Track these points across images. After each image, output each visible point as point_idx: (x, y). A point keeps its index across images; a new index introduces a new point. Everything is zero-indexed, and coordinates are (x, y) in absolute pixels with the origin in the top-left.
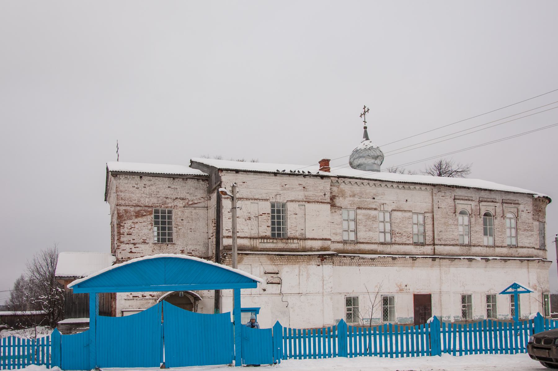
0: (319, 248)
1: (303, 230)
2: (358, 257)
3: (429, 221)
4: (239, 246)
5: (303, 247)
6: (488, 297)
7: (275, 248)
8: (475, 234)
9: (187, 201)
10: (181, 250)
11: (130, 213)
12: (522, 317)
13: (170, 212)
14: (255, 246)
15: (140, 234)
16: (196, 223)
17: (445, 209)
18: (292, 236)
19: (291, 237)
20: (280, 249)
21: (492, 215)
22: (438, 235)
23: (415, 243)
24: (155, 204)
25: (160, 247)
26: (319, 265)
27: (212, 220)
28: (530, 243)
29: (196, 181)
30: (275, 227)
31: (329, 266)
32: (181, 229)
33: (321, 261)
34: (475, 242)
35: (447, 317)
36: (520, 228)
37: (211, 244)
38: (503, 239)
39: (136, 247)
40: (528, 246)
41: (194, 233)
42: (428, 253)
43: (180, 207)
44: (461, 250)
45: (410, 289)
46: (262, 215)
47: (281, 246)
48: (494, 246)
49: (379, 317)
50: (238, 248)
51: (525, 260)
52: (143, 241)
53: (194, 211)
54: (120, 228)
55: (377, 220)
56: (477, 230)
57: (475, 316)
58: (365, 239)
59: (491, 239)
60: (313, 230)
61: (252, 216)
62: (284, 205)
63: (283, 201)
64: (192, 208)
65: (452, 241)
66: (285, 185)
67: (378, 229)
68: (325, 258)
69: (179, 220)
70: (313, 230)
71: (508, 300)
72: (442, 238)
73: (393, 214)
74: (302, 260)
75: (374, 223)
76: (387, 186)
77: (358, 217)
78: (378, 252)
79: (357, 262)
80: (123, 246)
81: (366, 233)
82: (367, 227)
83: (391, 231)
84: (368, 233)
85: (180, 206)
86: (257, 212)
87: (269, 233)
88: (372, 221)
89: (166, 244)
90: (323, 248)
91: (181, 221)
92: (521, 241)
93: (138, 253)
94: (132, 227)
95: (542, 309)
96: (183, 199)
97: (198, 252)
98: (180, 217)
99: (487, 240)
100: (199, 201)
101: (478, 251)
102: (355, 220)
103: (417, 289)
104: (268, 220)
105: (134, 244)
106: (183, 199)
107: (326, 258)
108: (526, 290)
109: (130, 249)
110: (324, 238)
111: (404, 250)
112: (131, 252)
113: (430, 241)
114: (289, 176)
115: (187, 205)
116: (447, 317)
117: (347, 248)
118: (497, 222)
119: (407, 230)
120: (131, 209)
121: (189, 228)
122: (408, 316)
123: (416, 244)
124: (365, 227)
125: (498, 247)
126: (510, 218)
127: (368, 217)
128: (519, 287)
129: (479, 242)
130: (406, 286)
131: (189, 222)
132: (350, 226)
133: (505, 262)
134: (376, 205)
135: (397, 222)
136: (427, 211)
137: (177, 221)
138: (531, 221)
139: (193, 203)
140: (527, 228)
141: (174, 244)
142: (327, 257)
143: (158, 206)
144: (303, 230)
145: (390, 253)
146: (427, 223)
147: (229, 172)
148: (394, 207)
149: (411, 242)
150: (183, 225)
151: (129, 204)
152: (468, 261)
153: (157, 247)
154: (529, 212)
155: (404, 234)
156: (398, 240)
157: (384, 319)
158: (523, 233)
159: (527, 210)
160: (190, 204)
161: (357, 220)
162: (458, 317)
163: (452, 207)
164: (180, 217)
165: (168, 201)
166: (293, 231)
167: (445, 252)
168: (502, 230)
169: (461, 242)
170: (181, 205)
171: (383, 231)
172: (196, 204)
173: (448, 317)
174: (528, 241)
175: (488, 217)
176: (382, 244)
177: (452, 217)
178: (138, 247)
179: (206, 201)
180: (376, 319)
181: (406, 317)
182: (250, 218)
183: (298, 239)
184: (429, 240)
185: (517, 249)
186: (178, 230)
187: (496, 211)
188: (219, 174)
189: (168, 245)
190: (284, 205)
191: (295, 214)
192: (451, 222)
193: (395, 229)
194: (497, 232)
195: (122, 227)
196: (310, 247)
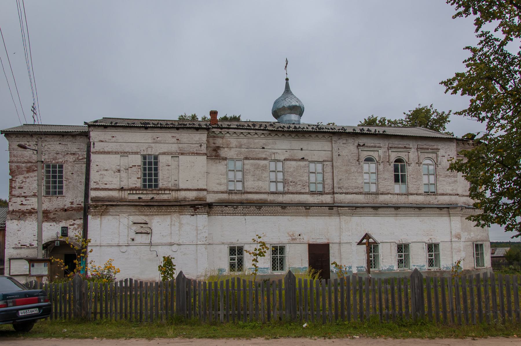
0: (194, 198)
1: (176, 181)
2: (241, 207)
3: (328, 169)
5: (175, 198)
6: (477, 246)
9: (77, 156)
10: (70, 202)
11: (22, 168)
12: (442, 267)
13: (61, 167)
14: (123, 197)
15: (31, 188)
17: (347, 157)
18: (164, 187)
19: (163, 188)
21: (405, 161)
22: (338, 183)
23: (311, 191)
24: (46, 160)
25: (50, 199)
26: (193, 215)
28: (453, 190)
31: (204, 216)
36: (440, 174)
38: (418, 186)
39: (27, 200)
40: (451, 192)
42: (327, 201)
43: (71, 162)
44: (366, 198)
45: (304, 239)
46: (132, 168)
48: (408, 194)
49: (267, 267)
52: (33, 194)
54: (12, 182)
55: (267, 170)
56: (386, 177)
57: (383, 267)
59: (403, 186)
60: (187, 181)
61: (122, 169)
62: (156, 158)
63: (155, 153)
65: (355, 189)
66: (157, 138)
68: (197, 208)
69: (69, 174)
70: (187, 181)
71: (425, 249)
72: (343, 186)
73: (285, 163)
75: (264, 172)
76: (278, 135)
79: (242, 211)
80: (14, 199)
82: (255, 176)
84: (257, 183)
85: (70, 161)
86: (127, 165)
87: (139, 184)
88: (261, 170)
89: (56, 196)
90: (198, 199)
91: (71, 175)
92: (442, 188)
93: (28, 205)
94: (24, 181)
95: (473, 260)
96: (74, 154)
98: (70, 171)
99: (398, 188)
101: (387, 199)
102: (242, 171)
103: (313, 239)
104: (139, 172)
105: (25, 197)
106: (74, 154)
107: (198, 208)
109: (21, 201)
111: (299, 199)
112: (22, 204)
113: (329, 189)
120: (23, 165)
121: (79, 181)
122: (302, 266)
123: (312, 193)
124: (253, 176)
125: (412, 194)
126: (428, 165)
127: (257, 167)
129: (389, 190)
130: (300, 235)
135: (290, 171)
136: (326, 159)
141: (64, 196)
143: (49, 162)
144: (176, 181)
145: (282, 202)
146: (327, 172)
148: (287, 155)
149: (307, 191)
150: (73, 179)
151: (21, 160)
153: (47, 199)
156: (291, 189)
157: (273, 268)
158: (443, 179)
162: (362, 267)
163: (355, 155)
164: (70, 171)
165: (58, 156)
167: (347, 201)
169: (366, 190)
170: (71, 160)
173: (348, 267)
174: (450, 188)
175: (399, 164)
177: (355, 164)
178: (28, 200)
180: (264, 268)
181: (299, 267)
182: (119, 170)
183: (170, 190)
184: (328, 189)
185: (436, 196)
186: (68, 183)
187: (410, 157)
189: (58, 198)
191: (167, 165)
192: (353, 169)
194: (411, 179)
195: (13, 182)
196: (183, 197)
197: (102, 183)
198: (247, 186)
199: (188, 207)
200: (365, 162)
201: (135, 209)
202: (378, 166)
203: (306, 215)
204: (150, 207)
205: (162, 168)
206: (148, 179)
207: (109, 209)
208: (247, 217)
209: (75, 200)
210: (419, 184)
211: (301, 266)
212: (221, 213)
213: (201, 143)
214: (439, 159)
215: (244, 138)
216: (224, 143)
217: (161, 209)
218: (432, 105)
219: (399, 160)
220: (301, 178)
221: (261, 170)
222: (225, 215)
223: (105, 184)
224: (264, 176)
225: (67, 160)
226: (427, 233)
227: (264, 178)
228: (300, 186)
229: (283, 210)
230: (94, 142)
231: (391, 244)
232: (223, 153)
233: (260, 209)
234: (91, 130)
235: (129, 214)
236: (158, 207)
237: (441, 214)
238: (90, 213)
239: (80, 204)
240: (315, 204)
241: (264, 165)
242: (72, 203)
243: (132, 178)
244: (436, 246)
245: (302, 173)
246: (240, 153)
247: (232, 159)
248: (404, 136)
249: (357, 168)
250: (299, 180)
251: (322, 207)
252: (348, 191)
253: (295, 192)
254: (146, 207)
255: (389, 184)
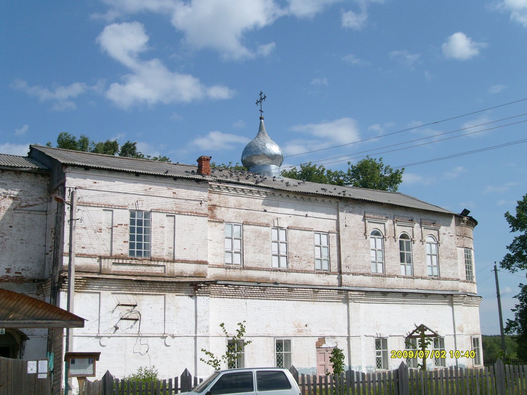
0: (192, 273)
1: (171, 248)
2: (243, 287)
4: (85, 267)
5: (170, 271)
7: (133, 271)
8: (390, 261)
10: (6, 269)
16: (30, 231)
19: (156, 257)
20: (140, 272)
21: (410, 237)
27: (52, 229)
29: (33, 176)
30: (135, 243)
32: (9, 239)
33: (194, 291)
34: (391, 271)
35: (357, 367)
36: (442, 254)
37: (49, 262)
40: (452, 277)
41: (26, 246)
42: (334, 283)
45: (312, 331)
47: (141, 269)
50: (75, 269)
51: (449, 295)
53: (28, 216)
56: (392, 255)
58: (254, 263)
62: (147, 214)
64: (26, 212)
65: (363, 268)
67: (270, 251)
68: (199, 286)
72: (350, 265)
74: (169, 289)
76: (282, 195)
77: (245, 234)
78: (271, 280)
79: (243, 293)
81: (256, 255)
83: (288, 254)
88: (263, 239)
97: (31, 273)
99: (402, 269)
100: (36, 203)
101: (394, 282)
107: (200, 287)
108: (433, 334)
110: (199, 259)
114: (155, 177)
115: (19, 207)
116: (357, 367)
117: (231, 274)
118: (415, 247)
119: (307, 253)
121: (19, 239)
122: (309, 366)
123: (319, 272)
127: (258, 235)
128: (427, 328)
129: (395, 271)
130: (306, 326)
131: (20, 231)
132: (234, 245)
133: (425, 297)
134: (268, 219)
135: (294, 242)
137: (3, 229)
138: (454, 246)
139: (27, 205)
140: (450, 255)
142: (202, 285)
144: (171, 248)
147: (76, 168)
149: (313, 269)
152: (381, 295)
154: (451, 236)
155: (303, 258)
156: (296, 266)
159: (449, 233)
160: (24, 205)
161: (244, 237)
162: (371, 367)
164: (8, 223)
166: (158, 249)
167: (355, 284)
168: (422, 257)
171: (277, 253)
172: (31, 206)
173: (358, 367)
174: (452, 272)
175: (404, 240)
176: (276, 270)
179: (46, 203)
181: (306, 367)
182: (101, 230)
186: (4, 240)
188: (63, 170)
190: (147, 214)
191: (161, 227)
192: (361, 244)
193: (293, 251)
194: (416, 258)
196: (180, 271)
197: (78, 247)
198: (246, 259)
199: (187, 285)
200: (372, 236)
201: (122, 285)
202: (385, 241)
203: (314, 300)
204: (141, 283)
205: (154, 230)
206: (137, 243)
207: (88, 284)
208: (248, 301)
209: (13, 266)
210: (424, 266)
211: (308, 367)
212: (218, 294)
213: (201, 200)
214: (441, 236)
215: (244, 196)
216: (221, 201)
217: (154, 286)
218: (381, 158)
219: (403, 236)
220: (306, 252)
221: (263, 239)
222: (223, 296)
223: (83, 248)
224: (265, 247)
225: (4, 207)
226: (433, 324)
227: (265, 249)
228: (305, 262)
229: (289, 293)
230: (70, 188)
231: (399, 338)
232: (219, 213)
233: (264, 290)
234: (68, 171)
235: (113, 292)
236: (151, 284)
237: (385, 300)
238: (64, 288)
239: (20, 273)
240: (321, 286)
241: (266, 233)
242: (8, 270)
243: (117, 241)
244: (385, 340)
245: (307, 246)
246: (240, 216)
247: (229, 223)
248: (409, 207)
249: (364, 242)
250: (304, 255)
251: (331, 291)
252: (356, 271)
253: (300, 269)
254: (136, 283)
255: (396, 264)
